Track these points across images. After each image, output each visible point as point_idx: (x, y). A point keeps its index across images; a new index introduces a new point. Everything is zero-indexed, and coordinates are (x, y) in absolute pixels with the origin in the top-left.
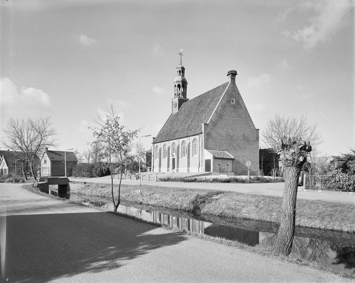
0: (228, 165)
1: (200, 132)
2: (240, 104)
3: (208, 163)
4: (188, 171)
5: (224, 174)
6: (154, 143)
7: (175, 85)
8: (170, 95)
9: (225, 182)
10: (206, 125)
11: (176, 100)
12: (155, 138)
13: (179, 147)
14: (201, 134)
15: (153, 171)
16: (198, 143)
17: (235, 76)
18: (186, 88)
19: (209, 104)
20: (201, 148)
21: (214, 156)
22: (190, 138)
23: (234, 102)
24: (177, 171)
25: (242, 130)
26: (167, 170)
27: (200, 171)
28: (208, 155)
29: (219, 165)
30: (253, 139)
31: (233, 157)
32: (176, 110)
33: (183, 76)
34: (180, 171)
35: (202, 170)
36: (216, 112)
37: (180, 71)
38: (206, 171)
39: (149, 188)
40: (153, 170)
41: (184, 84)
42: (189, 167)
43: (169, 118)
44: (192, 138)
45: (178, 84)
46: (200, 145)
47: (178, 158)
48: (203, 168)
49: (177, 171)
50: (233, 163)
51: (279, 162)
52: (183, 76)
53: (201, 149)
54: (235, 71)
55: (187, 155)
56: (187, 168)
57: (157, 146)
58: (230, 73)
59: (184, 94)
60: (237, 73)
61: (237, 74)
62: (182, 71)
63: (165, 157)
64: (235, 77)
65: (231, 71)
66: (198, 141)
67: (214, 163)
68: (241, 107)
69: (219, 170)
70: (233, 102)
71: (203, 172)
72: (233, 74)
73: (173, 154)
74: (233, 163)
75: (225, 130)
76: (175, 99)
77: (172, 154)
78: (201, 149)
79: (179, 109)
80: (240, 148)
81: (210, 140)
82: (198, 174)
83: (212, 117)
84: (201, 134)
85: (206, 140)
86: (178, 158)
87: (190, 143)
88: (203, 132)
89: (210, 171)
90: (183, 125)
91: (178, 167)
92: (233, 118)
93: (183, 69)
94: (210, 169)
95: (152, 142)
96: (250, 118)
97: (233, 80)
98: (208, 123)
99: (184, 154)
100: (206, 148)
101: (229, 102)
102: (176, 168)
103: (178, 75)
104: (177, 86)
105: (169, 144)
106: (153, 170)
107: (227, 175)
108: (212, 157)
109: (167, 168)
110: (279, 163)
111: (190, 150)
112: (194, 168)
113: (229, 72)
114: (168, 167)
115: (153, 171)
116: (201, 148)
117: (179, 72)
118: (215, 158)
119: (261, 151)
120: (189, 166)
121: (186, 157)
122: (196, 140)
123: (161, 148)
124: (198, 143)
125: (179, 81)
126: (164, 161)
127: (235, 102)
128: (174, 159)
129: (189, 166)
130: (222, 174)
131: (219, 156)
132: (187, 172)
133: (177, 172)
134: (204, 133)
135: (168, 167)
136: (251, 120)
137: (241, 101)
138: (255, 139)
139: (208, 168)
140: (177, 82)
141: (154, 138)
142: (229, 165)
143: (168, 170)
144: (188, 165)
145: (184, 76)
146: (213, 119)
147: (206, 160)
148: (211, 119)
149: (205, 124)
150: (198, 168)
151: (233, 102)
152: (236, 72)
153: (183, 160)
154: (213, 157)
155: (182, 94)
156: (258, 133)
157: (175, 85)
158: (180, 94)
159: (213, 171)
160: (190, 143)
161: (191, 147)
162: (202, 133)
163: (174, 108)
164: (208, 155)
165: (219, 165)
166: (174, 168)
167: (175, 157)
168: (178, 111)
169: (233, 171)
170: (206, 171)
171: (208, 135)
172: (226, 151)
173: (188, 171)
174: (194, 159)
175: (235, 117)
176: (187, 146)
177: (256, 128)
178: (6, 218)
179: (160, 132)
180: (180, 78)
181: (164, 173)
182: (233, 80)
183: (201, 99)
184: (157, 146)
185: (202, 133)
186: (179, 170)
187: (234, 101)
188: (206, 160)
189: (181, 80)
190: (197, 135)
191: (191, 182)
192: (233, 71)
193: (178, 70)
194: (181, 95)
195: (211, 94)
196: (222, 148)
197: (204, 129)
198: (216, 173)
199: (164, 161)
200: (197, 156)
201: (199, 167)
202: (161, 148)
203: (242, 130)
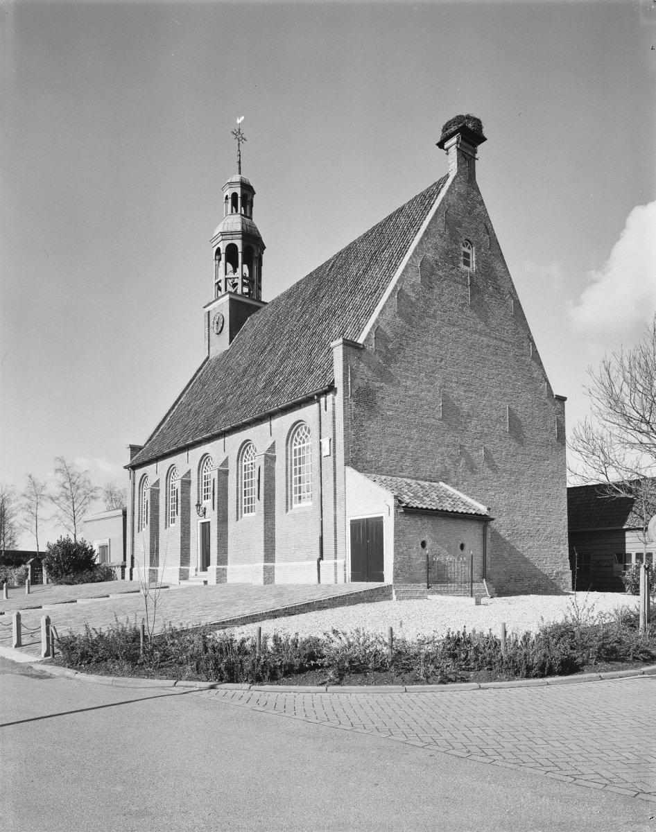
0: (462, 547)
1: (320, 386)
2: (495, 279)
3: (366, 539)
4: (269, 575)
5: (447, 593)
6: (133, 467)
7: (218, 251)
8: (204, 289)
9: (551, 673)
10: (351, 349)
11: (222, 306)
12: (140, 448)
13: (226, 473)
14: (330, 396)
15: (131, 579)
16: (312, 442)
17: (475, 146)
18: (260, 264)
19: (356, 282)
20: (328, 463)
21: (400, 502)
22: (276, 422)
23: (473, 265)
24: (221, 576)
25: (505, 395)
26: (178, 573)
27: (328, 578)
28: (369, 498)
29: (423, 544)
30: (546, 435)
31: (483, 509)
32: (222, 344)
33: (248, 215)
34: (231, 579)
35: (337, 572)
36: (399, 293)
37: (235, 195)
38: (356, 577)
39: (526, 408)
40: (131, 575)
41: (248, 250)
42: (273, 561)
43: (196, 375)
44: (283, 423)
45: (230, 242)
46: (326, 452)
47: (223, 520)
48: (340, 562)
49: (221, 576)
50: (484, 535)
51: (627, 534)
52: (246, 216)
53: (328, 469)
54: (475, 119)
55: (259, 505)
56: (261, 564)
57: (144, 477)
58: (453, 129)
59: (254, 282)
60: (485, 133)
61: (484, 139)
62: (244, 198)
63: (173, 521)
64: (475, 152)
65: (460, 119)
66: (315, 433)
67: (398, 533)
68: (497, 289)
69: (424, 571)
70: (467, 263)
71: (341, 580)
72: (468, 135)
73: (203, 506)
74: (484, 535)
75: (437, 383)
76: (217, 302)
77: (198, 505)
78: (328, 469)
79: (231, 339)
80: (494, 468)
81: (373, 426)
82: (319, 596)
83: (382, 312)
84: (325, 393)
85: (353, 422)
86: (223, 520)
87: (273, 446)
88: (339, 385)
89: (382, 580)
90: (247, 383)
91: (223, 560)
92: (468, 335)
93: (248, 190)
94: (380, 566)
95: (128, 461)
96: (534, 345)
97: (467, 159)
98: (361, 341)
99: (250, 501)
100: (356, 461)
101: (451, 258)
102: (213, 567)
103: (229, 212)
104: (223, 251)
105: (186, 462)
106: (131, 575)
107: (473, 600)
108: (392, 502)
109: (178, 567)
110: (627, 540)
111: (273, 478)
112: (294, 564)
113: (446, 128)
114: (185, 559)
115: (131, 579)
116: (328, 463)
117: (230, 201)
118: (407, 511)
119: (575, 495)
120: (269, 554)
121: (255, 518)
122: (302, 430)
123: (157, 483)
124: (312, 442)
125: (232, 233)
126: (170, 536)
127: (477, 263)
128: (205, 527)
129: (269, 554)
130: (439, 593)
131: (422, 501)
132: (260, 581)
133: (218, 581)
134: (345, 387)
135: (185, 559)
136: (536, 357)
137: (498, 266)
138: (553, 438)
139: (366, 557)
140: (223, 234)
141: (134, 449)
142: (466, 548)
143: (184, 576)
144: (266, 550)
145: (250, 218)
146: (383, 325)
147: (356, 525)
148: (377, 321)
149: (350, 345)
150: (316, 562)
151: (467, 263)
152: (478, 123)
153: (246, 528)
154: (397, 507)
155: (244, 284)
156: (562, 412)
157: (218, 251)
158: (237, 284)
159: (396, 576)
160: (273, 446)
161: (279, 466)
162: (331, 389)
163: (213, 336)
164: (369, 498)
165: (423, 544)
166: (208, 564)
167: (212, 517)
168: (227, 347)
169: (484, 575)
170: (356, 577)
171: (363, 400)
172: (441, 484)
173: (269, 575)
174: (297, 521)
175: (480, 334)
176: (260, 462)
177: (555, 393)
178: (229, 562)
179: (159, 427)
180: (234, 222)
181: (167, 587)
182: (467, 159)
183: (324, 283)
184: (144, 477)
185: (331, 389)
186: (229, 572)
187: (473, 258)
188: (356, 525)
189: (239, 228)
190: (308, 401)
191: (273, 678)
192: (468, 117)
193: (229, 193)
194: (239, 286)
195: (361, 246)
196: (426, 468)
197: (345, 368)
198: (410, 587)
199: (170, 536)
200: (308, 504)
201: (321, 558)
202: (157, 483)
203: (505, 395)
